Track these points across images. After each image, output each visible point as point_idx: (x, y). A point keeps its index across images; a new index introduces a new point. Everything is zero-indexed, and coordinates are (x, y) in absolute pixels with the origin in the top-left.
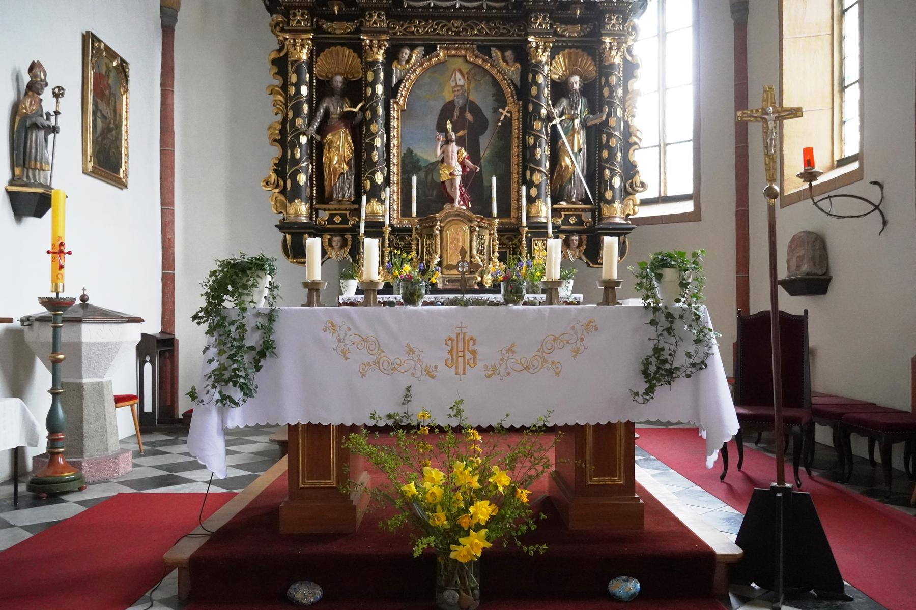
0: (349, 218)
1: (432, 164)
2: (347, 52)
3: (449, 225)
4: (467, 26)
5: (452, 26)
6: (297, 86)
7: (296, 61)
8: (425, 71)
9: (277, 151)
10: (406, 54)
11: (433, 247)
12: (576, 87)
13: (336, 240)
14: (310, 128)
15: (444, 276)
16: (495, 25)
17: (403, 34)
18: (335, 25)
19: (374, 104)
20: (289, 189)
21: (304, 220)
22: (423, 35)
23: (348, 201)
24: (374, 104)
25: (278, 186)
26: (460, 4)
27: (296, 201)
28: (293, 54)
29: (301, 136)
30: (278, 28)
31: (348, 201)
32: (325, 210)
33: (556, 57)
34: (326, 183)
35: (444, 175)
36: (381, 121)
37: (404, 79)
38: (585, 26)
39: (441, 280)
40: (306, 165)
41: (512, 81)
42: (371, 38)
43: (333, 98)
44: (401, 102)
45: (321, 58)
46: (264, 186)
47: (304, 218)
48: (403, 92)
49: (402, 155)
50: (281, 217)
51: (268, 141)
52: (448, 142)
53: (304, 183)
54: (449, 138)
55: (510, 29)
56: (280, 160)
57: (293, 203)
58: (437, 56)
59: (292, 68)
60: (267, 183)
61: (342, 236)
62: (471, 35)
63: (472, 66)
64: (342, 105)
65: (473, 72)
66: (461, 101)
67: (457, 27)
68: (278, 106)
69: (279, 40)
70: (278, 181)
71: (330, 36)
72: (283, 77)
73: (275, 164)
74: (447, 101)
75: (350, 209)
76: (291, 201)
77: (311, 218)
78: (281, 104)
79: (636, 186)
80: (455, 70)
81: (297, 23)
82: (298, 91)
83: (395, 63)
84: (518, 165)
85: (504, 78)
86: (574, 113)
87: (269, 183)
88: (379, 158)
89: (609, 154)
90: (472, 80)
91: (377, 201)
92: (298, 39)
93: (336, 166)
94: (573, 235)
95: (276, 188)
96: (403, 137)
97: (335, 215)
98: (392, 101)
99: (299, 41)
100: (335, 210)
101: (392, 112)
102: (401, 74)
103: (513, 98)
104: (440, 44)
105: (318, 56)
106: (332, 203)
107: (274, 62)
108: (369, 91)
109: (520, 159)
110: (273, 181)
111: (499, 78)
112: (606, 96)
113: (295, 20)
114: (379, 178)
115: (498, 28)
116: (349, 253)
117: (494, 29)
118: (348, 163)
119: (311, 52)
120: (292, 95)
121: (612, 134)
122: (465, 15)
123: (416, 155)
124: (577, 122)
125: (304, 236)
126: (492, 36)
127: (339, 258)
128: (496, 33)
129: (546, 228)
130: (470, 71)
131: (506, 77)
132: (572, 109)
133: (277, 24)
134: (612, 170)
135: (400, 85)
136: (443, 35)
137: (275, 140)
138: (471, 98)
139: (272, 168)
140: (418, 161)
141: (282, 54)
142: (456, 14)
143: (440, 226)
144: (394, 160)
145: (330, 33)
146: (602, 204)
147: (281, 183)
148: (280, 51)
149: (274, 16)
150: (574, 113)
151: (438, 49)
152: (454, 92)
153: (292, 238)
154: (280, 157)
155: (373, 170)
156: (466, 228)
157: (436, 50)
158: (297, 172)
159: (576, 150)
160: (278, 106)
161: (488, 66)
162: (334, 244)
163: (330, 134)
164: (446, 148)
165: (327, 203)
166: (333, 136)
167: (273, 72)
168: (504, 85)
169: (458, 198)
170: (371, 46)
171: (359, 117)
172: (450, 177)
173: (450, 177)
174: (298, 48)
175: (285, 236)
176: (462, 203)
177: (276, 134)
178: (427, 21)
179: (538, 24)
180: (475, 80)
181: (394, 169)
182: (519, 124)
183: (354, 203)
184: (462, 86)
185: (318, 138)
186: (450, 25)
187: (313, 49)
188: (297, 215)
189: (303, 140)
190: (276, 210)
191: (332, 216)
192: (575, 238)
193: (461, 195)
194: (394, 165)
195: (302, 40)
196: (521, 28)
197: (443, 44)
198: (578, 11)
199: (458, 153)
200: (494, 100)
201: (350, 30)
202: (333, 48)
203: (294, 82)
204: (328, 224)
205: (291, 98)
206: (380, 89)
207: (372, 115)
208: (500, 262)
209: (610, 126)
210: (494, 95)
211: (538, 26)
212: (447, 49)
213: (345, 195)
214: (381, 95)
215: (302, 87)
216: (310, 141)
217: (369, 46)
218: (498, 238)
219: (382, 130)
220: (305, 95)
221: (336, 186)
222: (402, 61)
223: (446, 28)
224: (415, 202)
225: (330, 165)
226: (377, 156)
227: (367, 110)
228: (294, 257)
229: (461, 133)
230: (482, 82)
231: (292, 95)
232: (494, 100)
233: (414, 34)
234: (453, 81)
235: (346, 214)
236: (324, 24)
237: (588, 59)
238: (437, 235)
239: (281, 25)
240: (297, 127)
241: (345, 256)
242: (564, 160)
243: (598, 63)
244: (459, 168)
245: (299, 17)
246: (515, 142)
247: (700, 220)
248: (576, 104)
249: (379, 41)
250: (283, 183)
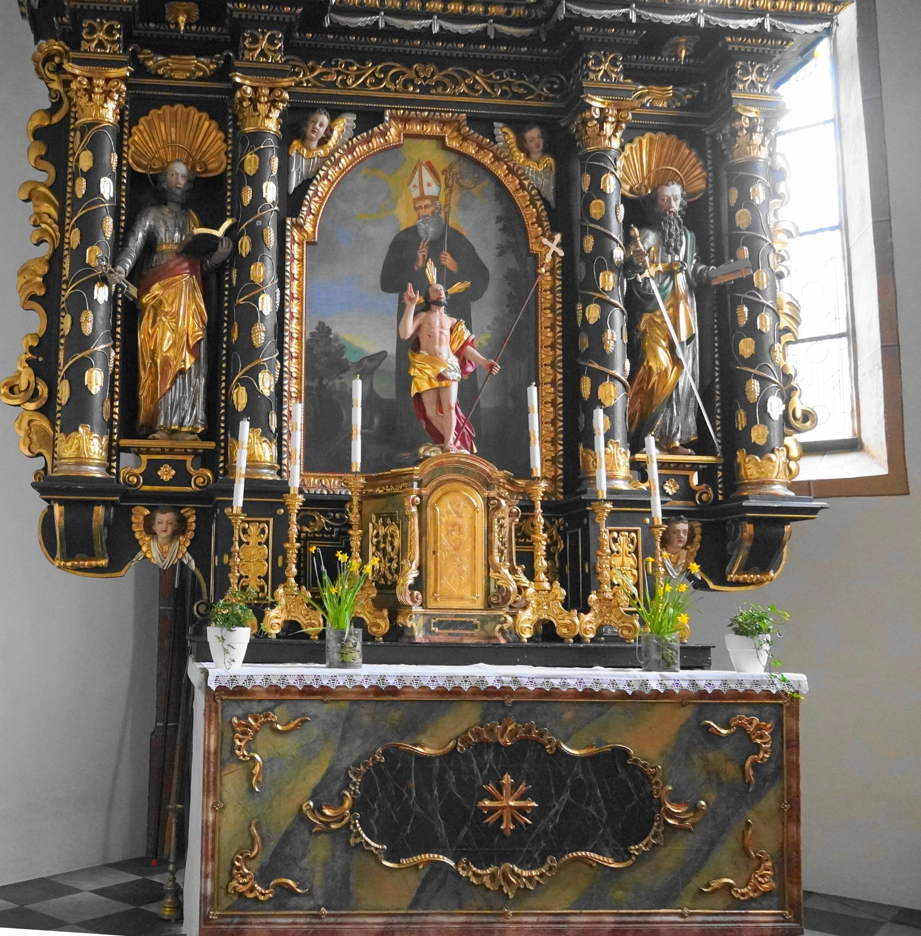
0: (191, 470)
1: (371, 358)
2: (197, 117)
3: (439, 492)
4: (446, 76)
5: (414, 75)
6: (93, 178)
7: (91, 125)
8: (356, 165)
9: (36, 322)
10: (321, 125)
11: (397, 542)
12: (676, 207)
13: (164, 520)
14: (119, 268)
15: (428, 612)
16: (502, 78)
17: (314, 86)
18: (172, 62)
19: (259, 223)
20: (64, 401)
21: (96, 472)
22: (353, 89)
23: (192, 433)
24: (259, 223)
25: (35, 395)
26: (441, 27)
27: (81, 429)
28: (86, 112)
29: (96, 287)
30: (50, 66)
31: (192, 433)
32: (138, 452)
33: (637, 140)
34: (143, 393)
35: (422, 383)
36: (270, 257)
37: (314, 177)
38: (684, 90)
39: (421, 622)
40: (105, 348)
41: (539, 193)
42: (256, 84)
43: (166, 210)
44: (308, 227)
45: (141, 127)
46: (5, 395)
47: (94, 468)
48: (312, 205)
49: (308, 337)
50: (39, 463)
51: (17, 299)
52: (427, 306)
53: (98, 389)
54: (433, 297)
55: (532, 87)
56: (41, 340)
57: (73, 434)
58: (383, 134)
59: (81, 141)
60: (11, 390)
61: (177, 510)
62: (454, 95)
63: (453, 158)
64: (184, 225)
65: (456, 169)
66: (431, 229)
67: (425, 79)
68: (43, 226)
69: (50, 89)
70: (36, 384)
71: (161, 82)
72: (56, 168)
73: (31, 349)
74: (403, 228)
75: (195, 452)
76: (70, 428)
77: (109, 470)
78: (49, 221)
79: (795, 419)
80: (419, 163)
81: (97, 46)
82: (93, 189)
83: (296, 143)
84: (553, 365)
85: (521, 184)
86: (673, 260)
87: (16, 389)
88: (266, 339)
89: (759, 346)
90: (456, 187)
91: (263, 435)
92: (99, 78)
93: (171, 354)
94: (679, 520)
95: (30, 400)
96: (309, 301)
97: (161, 463)
98: (289, 222)
99: (102, 82)
100: (163, 451)
101: (288, 245)
102: (308, 166)
103: (541, 225)
104: (391, 109)
105: (134, 122)
106: (156, 435)
107: (38, 134)
108: (248, 195)
109: (559, 352)
110: (24, 386)
111: (511, 184)
112: (743, 227)
113: (93, 41)
114: (266, 383)
115: (509, 84)
116: (189, 549)
117: (501, 85)
118: (194, 351)
119: (121, 110)
120: (80, 196)
121: (763, 304)
122: (443, 53)
123: (337, 339)
124: (681, 278)
125: (96, 508)
126: (496, 98)
127: (167, 560)
128: (504, 94)
129: (648, 504)
130: (450, 167)
131: (526, 182)
132: (668, 252)
133: (49, 58)
134: (764, 381)
135: (308, 188)
136: (396, 91)
137: (33, 297)
138: (453, 223)
139: (24, 357)
140: (341, 350)
141: (56, 119)
142: (425, 51)
143: (420, 496)
144: (293, 347)
145: (161, 77)
146: (741, 455)
147: (43, 389)
148: (51, 112)
149: (42, 42)
150: (673, 260)
151: (387, 118)
152: (416, 209)
153: (66, 515)
154: (41, 335)
155: (254, 364)
156: (478, 501)
157: (382, 121)
158: (85, 365)
159: (684, 338)
160: (43, 226)
161: (487, 159)
162: (158, 528)
163: (156, 286)
164: (427, 318)
165: (145, 437)
166: (164, 288)
167: (33, 156)
168: (521, 199)
169: (453, 437)
170: (254, 101)
171: (225, 248)
172: (436, 384)
173: (436, 384)
174: (97, 97)
175: (51, 508)
176: (459, 443)
177: (36, 284)
178: (363, 62)
179: (601, 73)
180: (461, 186)
181: (292, 366)
182: (554, 280)
183: (204, 437)
184: (434, 199)
185: (133, 291)
186: (410, 74)
187: (125, 108)
188: (81, 461)
189: (101, 294)
190: (29, 450)
191: (154, 466)
192: (683, 526)
193: (458, 428)
194: (291, 357)
195: (108, 80)
196: (555, 86)
197: (397, 109)
198: (684, 52)
199: (451, 330)
200: (500, 230)
201: (205, 72)
202: (166, 108)
203: (85, 169)
204: (143, 484)
205: (77, 203)
206: (270, 191)
207: (253, 244)
208: (551, 583)
209: (757, 289)
210: (499, 219)
211: (602, 77)
212: (405, 120)
213: (183, 419)
214: (273, 203)
215: (102, 180)
216: (113, 298)
217: (250, 99)
218: (545, 525)
219: (272, 280)
220: (108, 198)
221: (166, 401)
222: (312, 140)
223: (402, 79)
224: (359, 436)
225: (154, 352)
226: (263, 334)
227: (242, 235)
228: (69, 555)
229: (457, 287)
230: (474, 190)
231: (80, 196)
232: (500, 230)
233: (336, 87)
234: (415, 186)
235: (185, 461)
236: (149, 59)
237: (690, 153)
238: (412, 515)
239: (57, 60)
240: (88, 265)
241: (180, 556)
242: (656, 356)
243: (710, 162)
244: (454, 362)
245: (101, 35)
246: (545, 318)
247: (908, 494)
248: (676, 241)
249: (272, 90)
250: (46, 391)
